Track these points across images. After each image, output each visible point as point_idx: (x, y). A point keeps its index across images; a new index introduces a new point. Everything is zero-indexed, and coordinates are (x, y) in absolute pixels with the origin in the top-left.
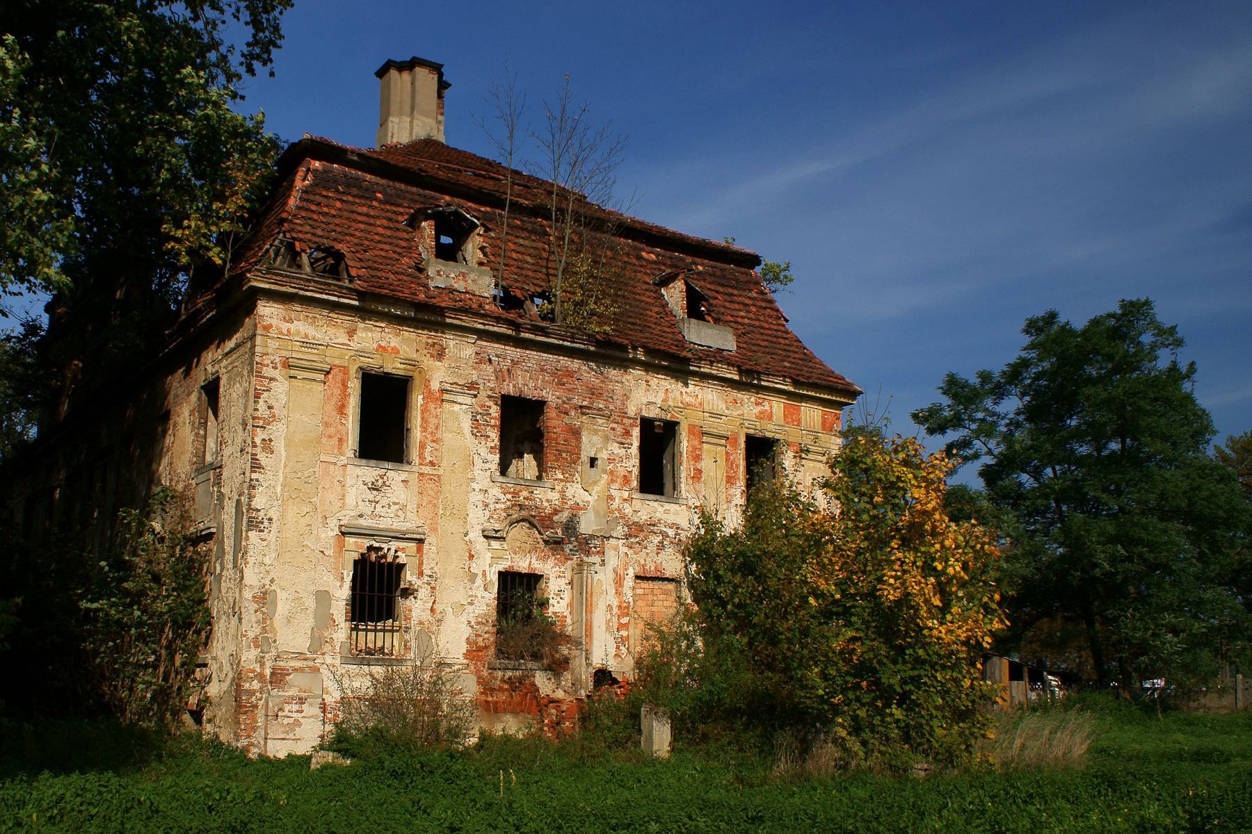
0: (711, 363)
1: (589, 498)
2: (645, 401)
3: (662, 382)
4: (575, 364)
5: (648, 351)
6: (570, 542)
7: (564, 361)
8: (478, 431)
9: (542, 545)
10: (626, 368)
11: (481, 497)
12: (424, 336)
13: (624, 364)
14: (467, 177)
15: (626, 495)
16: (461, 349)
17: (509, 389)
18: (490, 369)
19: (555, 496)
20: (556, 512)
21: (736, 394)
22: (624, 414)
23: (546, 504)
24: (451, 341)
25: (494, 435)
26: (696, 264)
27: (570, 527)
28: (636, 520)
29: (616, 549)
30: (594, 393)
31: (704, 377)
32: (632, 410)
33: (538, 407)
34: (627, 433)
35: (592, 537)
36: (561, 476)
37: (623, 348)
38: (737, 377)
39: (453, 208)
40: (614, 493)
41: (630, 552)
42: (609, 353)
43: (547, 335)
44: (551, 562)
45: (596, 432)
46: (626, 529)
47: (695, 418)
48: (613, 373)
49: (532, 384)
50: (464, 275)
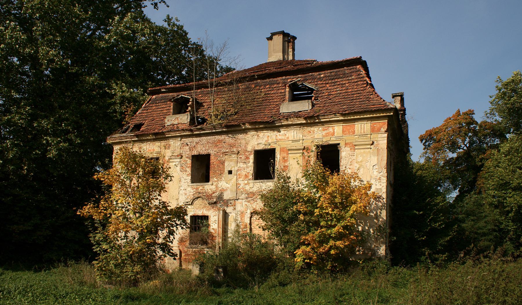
0: (287, 119)
1: (229, 186)
2: (256, 143)
3: (266, 134)
4: (223, 137)
5: (251, 123)
6: (220, 203)
7: (218, 137)
8: (183, 170)
9: (208, 205)
10: (246, 133)
11: (184, 191)
12: (163, 143)
13: (245, 131)
14: (273, 70)
15: (246, 182)
16: (175, 144)
17: (195, 153)
18: (187, 147)
19: (213, 187)
20: (214, 193)
21: (309, 129)
22: (246, 151)
23: (209, 191)
24: (171, 142)
25: (189, 170)
26: (320, 74)
27: (220, 197)
28: (251, 191)
29: (242, 203)
30: (231, 146)
31: (288, 126)
32: (250, 148)
33: (207, 157)
34: (247, 158)
35: (230, 200)
36: (216, 180)
37: (239, 126)
38: (304, 122)
39: (180, 96)
40: (240, 182)
41: (248, 204)
42: (233, 129)
43: (204, 130)
44: (212, 210)
45: (231, 161)
46: (246, 195)
47: (284, 145)
48: (240, 136)
49: (204, 149)
50: (177, 118)
